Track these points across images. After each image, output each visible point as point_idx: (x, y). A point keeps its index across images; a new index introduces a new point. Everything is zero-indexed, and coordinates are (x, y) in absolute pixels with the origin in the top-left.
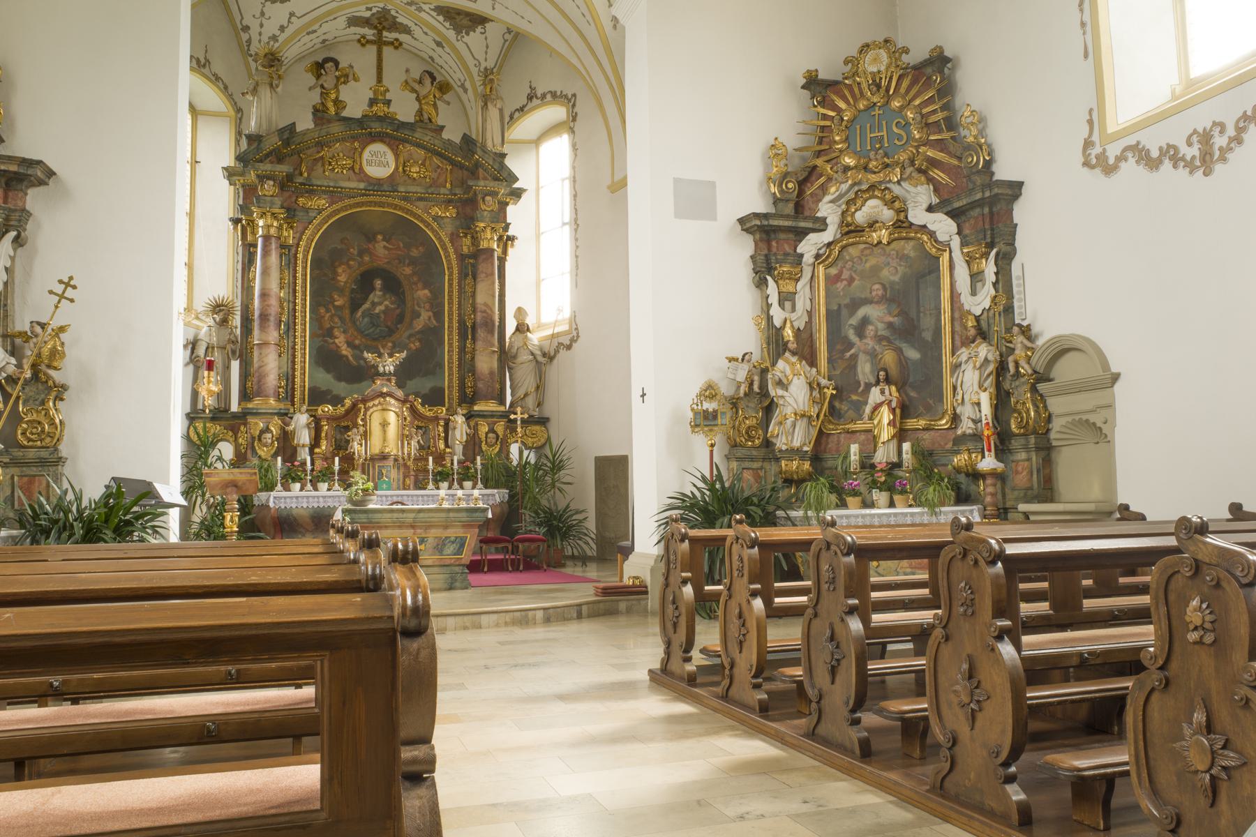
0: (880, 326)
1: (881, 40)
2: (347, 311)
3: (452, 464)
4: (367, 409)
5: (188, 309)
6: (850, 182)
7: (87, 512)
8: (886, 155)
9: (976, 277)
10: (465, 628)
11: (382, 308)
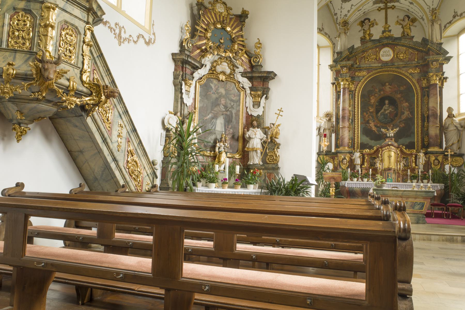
2: (375, 114)
3: (418, 173)
4: (382, 151)
5: (318, 116)
7: (286, 185)
10: (424, 240)
11: (388, 111)
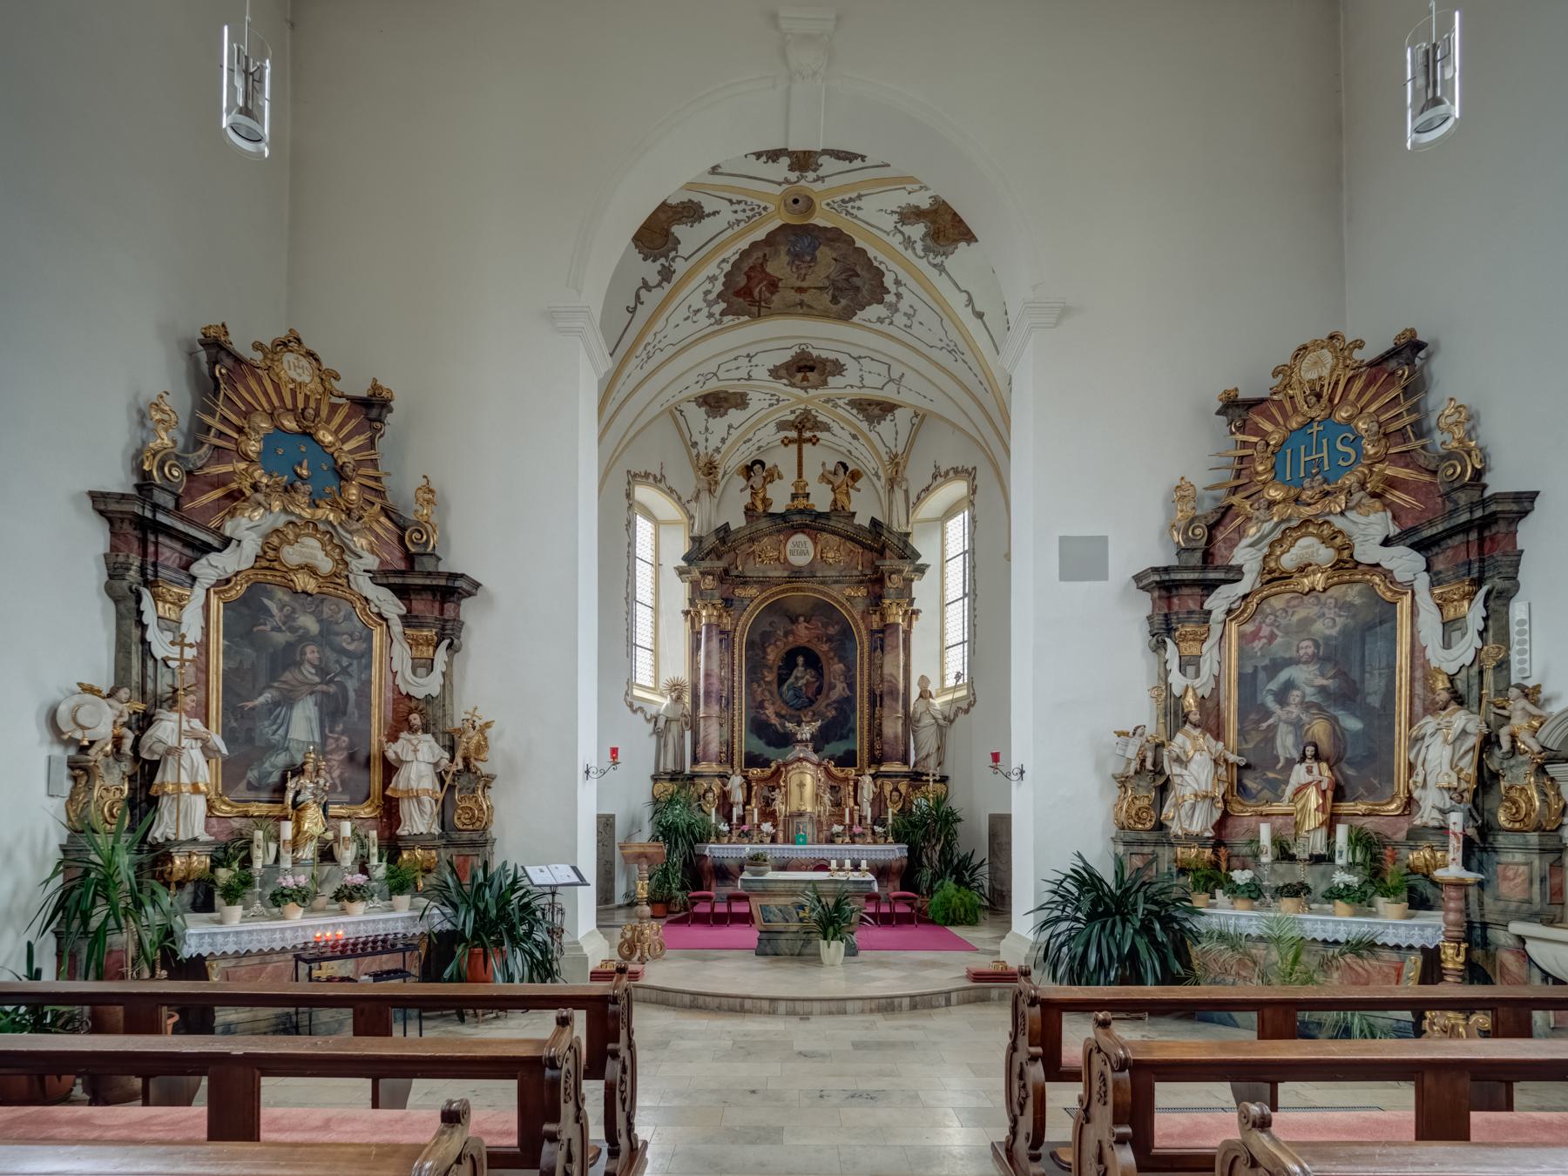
0: (1309, 690)
1: (1325, 337)
2: (775, 686)
4: (787, 772)
6: (1276, 519)
8: (1326, 481)
9: (1451, 627)
10: (831, 1013)
11: (804, 681)
